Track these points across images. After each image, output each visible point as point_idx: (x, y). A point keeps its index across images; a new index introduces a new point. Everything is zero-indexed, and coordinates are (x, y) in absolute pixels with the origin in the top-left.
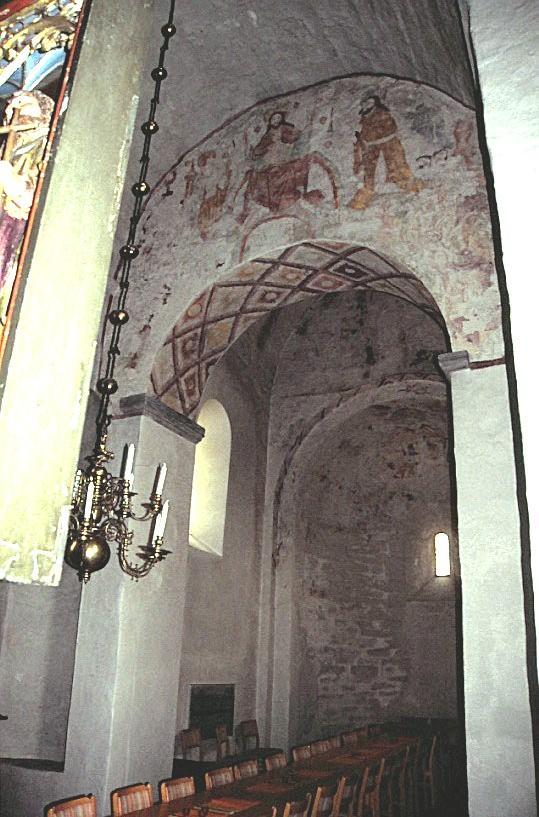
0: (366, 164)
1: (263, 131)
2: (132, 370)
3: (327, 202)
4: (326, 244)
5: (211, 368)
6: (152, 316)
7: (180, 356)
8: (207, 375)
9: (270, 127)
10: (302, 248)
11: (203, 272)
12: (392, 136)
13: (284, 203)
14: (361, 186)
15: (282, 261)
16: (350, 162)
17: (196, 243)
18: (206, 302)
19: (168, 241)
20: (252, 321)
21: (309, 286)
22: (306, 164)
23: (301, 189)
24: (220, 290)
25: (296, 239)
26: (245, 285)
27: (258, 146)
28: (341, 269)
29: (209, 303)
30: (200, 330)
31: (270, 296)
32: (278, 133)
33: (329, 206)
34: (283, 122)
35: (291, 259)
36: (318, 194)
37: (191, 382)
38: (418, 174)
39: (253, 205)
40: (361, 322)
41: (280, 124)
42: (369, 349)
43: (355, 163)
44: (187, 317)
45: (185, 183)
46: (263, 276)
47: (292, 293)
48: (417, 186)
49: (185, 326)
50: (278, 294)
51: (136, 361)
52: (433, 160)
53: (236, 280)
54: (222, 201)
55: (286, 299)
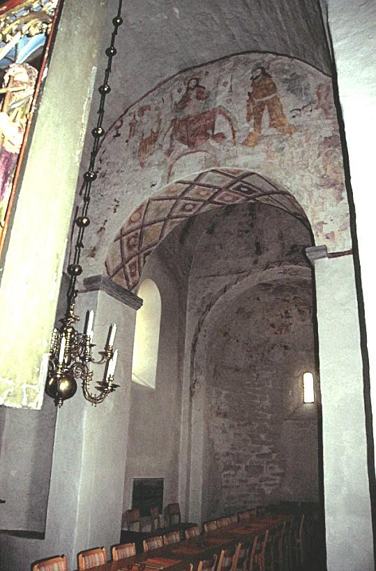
0: (255, 115)
1: (184, 92)
2: (92, 259)
4: (227, 170)
5: (147, 257)
6: (106, 221)
7: (125, 249)
8: (145, 262)
9: (188, 89)
10: (211, 173)
12: (274, 95)
13: (198, 142)
14: (252, 130)
15: (197, 182)
16: (244, 113)
18: (144, 211)
19: (117, 168)
20: (176, 225)
21: (216, 200)
22: (213, 115)
23: (210, 132)
24: (153, 202)
25: (207, 167)
26: (171, 199)
27: (180, 102)
28: (238, 188)
29: (146, 212)
30: (139, 230)
31: (188, 207)
32: (194, 93)
33: (229, 144)
34: (197, 85)
35: (203, 181)
36: (222, 136)
37: (133, 267)
38: (292, 122)
39: (177, 143)
40: (252, 225)
41: (195, 86)
42: (257, 244)
43: (248, 114)
44: (130, 222)
46: (183, 193)
47: (204, 204)
48: (291, 130)
49: (129, 228)
50: (194, 205)
51: (95, 252)
52: (302, 112)
53: (164, 195)
55: (199, 209)
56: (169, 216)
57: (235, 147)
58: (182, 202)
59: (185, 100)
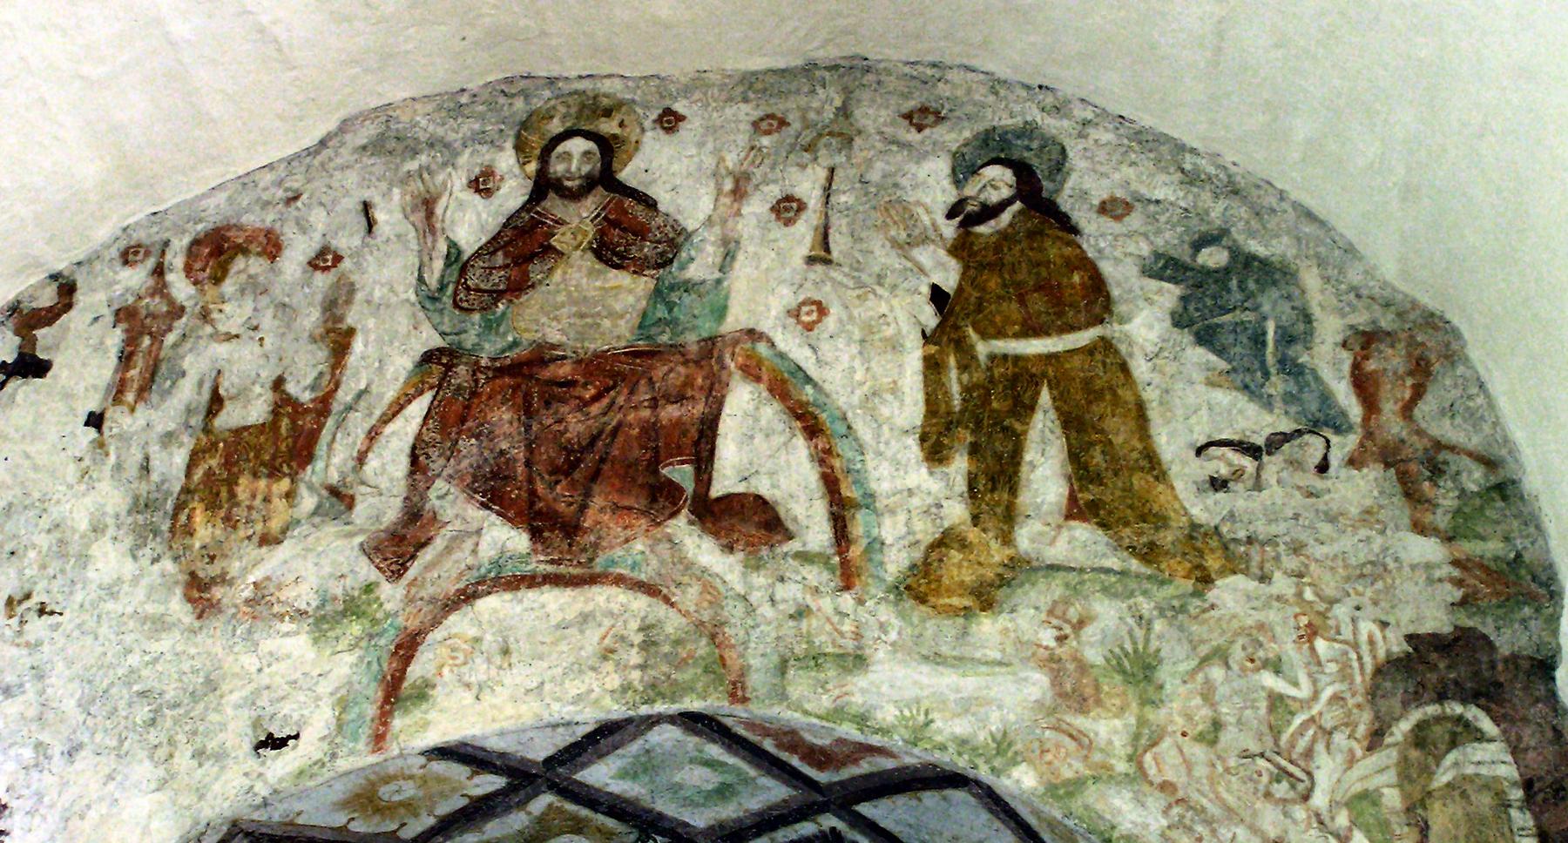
0: (976, 427)
3: (805, 557)
9: (544, 186)
11: (183, 760)
13: (597, 511)
14: (957, 512)
16: (910, 408)
17: (159, 625)
33: (814, 574)
35: (601, 774)
38: (1203, 509)
39: (452, 504)
41: (589, 184)
45: (115, 339)
48: (1205, 556)
54: (302, 451)
57: (847, 601)
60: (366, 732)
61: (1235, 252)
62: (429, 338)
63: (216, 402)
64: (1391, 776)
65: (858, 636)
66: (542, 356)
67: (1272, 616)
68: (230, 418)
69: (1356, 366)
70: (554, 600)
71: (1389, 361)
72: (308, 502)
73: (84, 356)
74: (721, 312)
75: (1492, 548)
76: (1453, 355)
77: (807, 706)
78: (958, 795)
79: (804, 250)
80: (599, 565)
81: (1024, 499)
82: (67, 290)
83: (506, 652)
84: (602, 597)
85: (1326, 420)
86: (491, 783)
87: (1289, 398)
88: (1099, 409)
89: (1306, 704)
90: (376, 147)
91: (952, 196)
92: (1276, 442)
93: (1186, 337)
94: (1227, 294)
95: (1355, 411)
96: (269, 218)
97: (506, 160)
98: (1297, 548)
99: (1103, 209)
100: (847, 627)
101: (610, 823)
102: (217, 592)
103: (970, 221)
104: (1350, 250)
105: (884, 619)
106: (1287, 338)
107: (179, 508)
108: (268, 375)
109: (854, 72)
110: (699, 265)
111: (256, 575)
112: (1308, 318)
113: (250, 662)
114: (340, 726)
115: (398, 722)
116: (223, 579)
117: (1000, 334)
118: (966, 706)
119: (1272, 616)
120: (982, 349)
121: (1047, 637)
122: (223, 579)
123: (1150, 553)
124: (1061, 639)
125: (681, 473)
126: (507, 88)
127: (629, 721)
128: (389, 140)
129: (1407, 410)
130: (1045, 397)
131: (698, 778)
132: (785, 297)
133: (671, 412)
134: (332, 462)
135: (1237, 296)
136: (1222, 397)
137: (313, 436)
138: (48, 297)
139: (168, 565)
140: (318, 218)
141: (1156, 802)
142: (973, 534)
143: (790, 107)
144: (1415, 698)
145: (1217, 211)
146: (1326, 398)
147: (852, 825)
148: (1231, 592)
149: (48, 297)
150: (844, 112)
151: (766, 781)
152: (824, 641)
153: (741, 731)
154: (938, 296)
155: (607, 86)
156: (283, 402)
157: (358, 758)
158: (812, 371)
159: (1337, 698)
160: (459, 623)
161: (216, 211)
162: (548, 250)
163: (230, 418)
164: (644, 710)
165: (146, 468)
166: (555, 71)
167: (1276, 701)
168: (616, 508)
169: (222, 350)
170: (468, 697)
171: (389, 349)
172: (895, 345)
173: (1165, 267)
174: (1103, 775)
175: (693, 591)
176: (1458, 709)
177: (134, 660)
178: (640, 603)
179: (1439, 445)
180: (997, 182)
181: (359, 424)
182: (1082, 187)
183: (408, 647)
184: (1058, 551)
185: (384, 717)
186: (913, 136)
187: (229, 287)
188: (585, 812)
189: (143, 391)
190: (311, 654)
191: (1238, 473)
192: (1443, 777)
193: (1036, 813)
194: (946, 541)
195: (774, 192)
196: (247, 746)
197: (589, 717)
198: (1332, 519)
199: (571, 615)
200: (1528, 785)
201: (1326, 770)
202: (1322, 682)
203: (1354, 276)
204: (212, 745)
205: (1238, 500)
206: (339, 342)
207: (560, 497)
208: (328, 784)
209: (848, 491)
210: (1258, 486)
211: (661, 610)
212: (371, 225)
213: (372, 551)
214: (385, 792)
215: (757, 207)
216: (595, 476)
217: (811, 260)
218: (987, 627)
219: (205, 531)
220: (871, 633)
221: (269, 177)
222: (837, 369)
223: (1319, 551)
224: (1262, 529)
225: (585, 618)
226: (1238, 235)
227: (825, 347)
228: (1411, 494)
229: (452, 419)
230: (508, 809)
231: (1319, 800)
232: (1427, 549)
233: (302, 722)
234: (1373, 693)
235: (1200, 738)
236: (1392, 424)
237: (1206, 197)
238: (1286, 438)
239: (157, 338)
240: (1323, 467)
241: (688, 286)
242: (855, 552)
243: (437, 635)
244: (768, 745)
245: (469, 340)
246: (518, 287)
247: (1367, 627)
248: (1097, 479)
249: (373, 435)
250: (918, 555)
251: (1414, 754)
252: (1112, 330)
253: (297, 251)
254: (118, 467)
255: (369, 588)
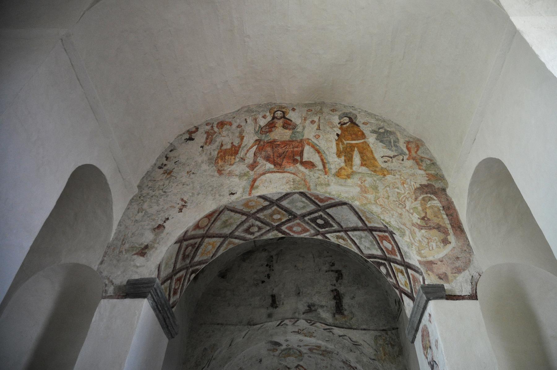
0: (346, 153)
2: (142, 258)
3: (319, 170)
6: (168, 219)
7: (264, 231)
9: (274, 118)
10: (297, 196)
11: (217, 196)
12: (363, 141)
13: (285, 162)
14: (343, 165)
16: (334, 150)
17: (213, 176)
18: (213, 219)
19: (188, 169)
21: (284, 228)
24: (227, 212)
28: (314, 220)
29: (214, 221)
33: (320, 172)
35: (284, 203)
38: (384, 165)
39: (260, 160)
40: (269, 276)
41: (281, 118)
42: (273, 297)
45: (205, 136)
46: (258, 211)
48: (384, 172)
49: (193, 233)
50: (260, 229)
51: (146, 251)
52: (394, 160)
53: (239, 207)
54: (236, 153)
55: (262, 235)
56: (231, 235)
57: (326, 176)
58: (252, 221)
59: (271, 126)
60: (248, 193)
61: (385, 130)
62: (256, 138)
63: (222, 145)
64: (419, 205)
65: (328, 181)
66: (274, 141)
67: (396, 181)
68: (224, 147)
69: (407, 146)
70: (278, 175)
71: (412, 146)
72: (237, 160)
73: (200, 138)
74: (303, 136)
75: (433, 172)
76: (423, 144)
77: (321, 191)
78: (345, 207)
79: (316, 128)
80: (285, 170)
81: (354, 163)
82: (197, 129)
83: (271, 182)
84: (286, 175)
85: (402, 153)
86: (267, 203)
87: (396, 150)
88: (364, 151)
89: (403, 194)
90: (247, 111)
91: (339, 121)
92: (394, 156)
93: (378, 141)
94: (384, 135)
95: (407, 152)
96: (230, 120)
97: (268, 114)
98: (400, 171)
99: (363, 123)
100: (326, 180)
101: (284, 212)
102: (223, 172)
103: (342, 125)
104: (404, 130)
105: (332, 179)
106: (395, 142)
107: (216, 160)
108: (230, 142)
109: (323, 104)
110: (299, 129)
111: (229, 169)
112: (398, 139)
113: (228, 182)
114: (244, 191)
115: (253, 191)
116: (224, 170)
117: (348, 140)
118: (346, 192)
119: (396, 181)
120: (345, 142)
121: (359, 183)
122: (224, 170)
123: (375, 171)
124: (362, 183)
125: (298, 158)
126: (268, 104)
127: (291, 193)
128: (249, 110)
129: (416, 152)
130: (356, 149)
131: (300, 204)
132: (313, 134)
133: (296, 149)
134: (241, 154)
135: (386, 136)
136: (385, 150)
137: (238, 151)
138: (194, 129)
139: (214, 168)
140: (238, 121)
141: (379, 208)
142: (346, 168)
143: (313, 108)
144: (422, 193)
145: (382, 124)
146: (402, 150)
147: (325, 214)
148: (389, 177)
149: (194, 129)
150: (321, 109)
151: (312, 205)
152: (323, 182)
153: (309, 195)
154: (338, 135)
155: (283, 104)
156: (233, 145)
157: (246, 196)
158: (318, 144)
159: (409, 193)
160: (263, 177)
161: (221, 119)
162: (275, 126)
163: (224, 147)
164: (294, 191)
165: (210, 154)
166: (275, 102)
167: (398, 193)
168: (287, 162)
169: (223, 138)
170: (265, 188)
171: (250, 139)
172: (331, 141)
173: (374, 132)
174: (370, 203)
175: (301, 174)
176: (430, 195)
177: (209, 181)
178: (292, 176)
179: (422, 157)
180: (346, 120)
181: (245, 149)
182: (359, 120)
183: (254, 181)
184: (360, 171)
185: (251, 191)
186: (332, 113)
187: (223, 130)
188: (281, 210)
189: (210, 143)
190: (238, 181)
191: (389, 161)
192: (428, 205)
193: (359, 209)
194: (341, 168)
195: (311, 120)
196: (228, 194)
197: (284, 192)
198: (405, 167)
199: (281, 177)
200: (443, 207)
201: (408, 204)
202: (406, 191)
203: (405, 133)
204: (222, 194)
205: (389, 164)
206: (242, 138)
207: (279, 160)
208: (241, 201)
209: (325, 161)
210: (392, 162)
211: (296, 177)
212: (246, 122)
213: (248, 167)
214: (250, 204)
215: (308, 122)
216: (284, 158)
217: (317, 129)
218: (349, 181)
219: (220, 163)
220: (330, 181)
221: (230, 115)
222: (322, 144)
223: (403, 172)
224: (393, 168)
225: (283, 177)
226: (386, 128)
227: (320, 141)
228: (418, 164)
229: (261, 149)
230: (268, 209)
231: (407, 208)
232: (422, 172)
233: (237, 191)
234: (415, 193)
235: (386, 198)
236: (413, 154)
237: (380, 122)
238: (396, 156)
239: (212, 136)
240: (403, 160)
241: (298, 132)
242: (327, 170)
243: (260, 179)
244: (313, 198)
245: (263, 138)
246: (270, 131)
247: (412, 183)
248: (366, 161)
249: (248, 151)
250: (337, 170)
251: (423, 202)
252: (366, 140)
253: (234, 125)
254: (206, 154)
255: (248, 172)
